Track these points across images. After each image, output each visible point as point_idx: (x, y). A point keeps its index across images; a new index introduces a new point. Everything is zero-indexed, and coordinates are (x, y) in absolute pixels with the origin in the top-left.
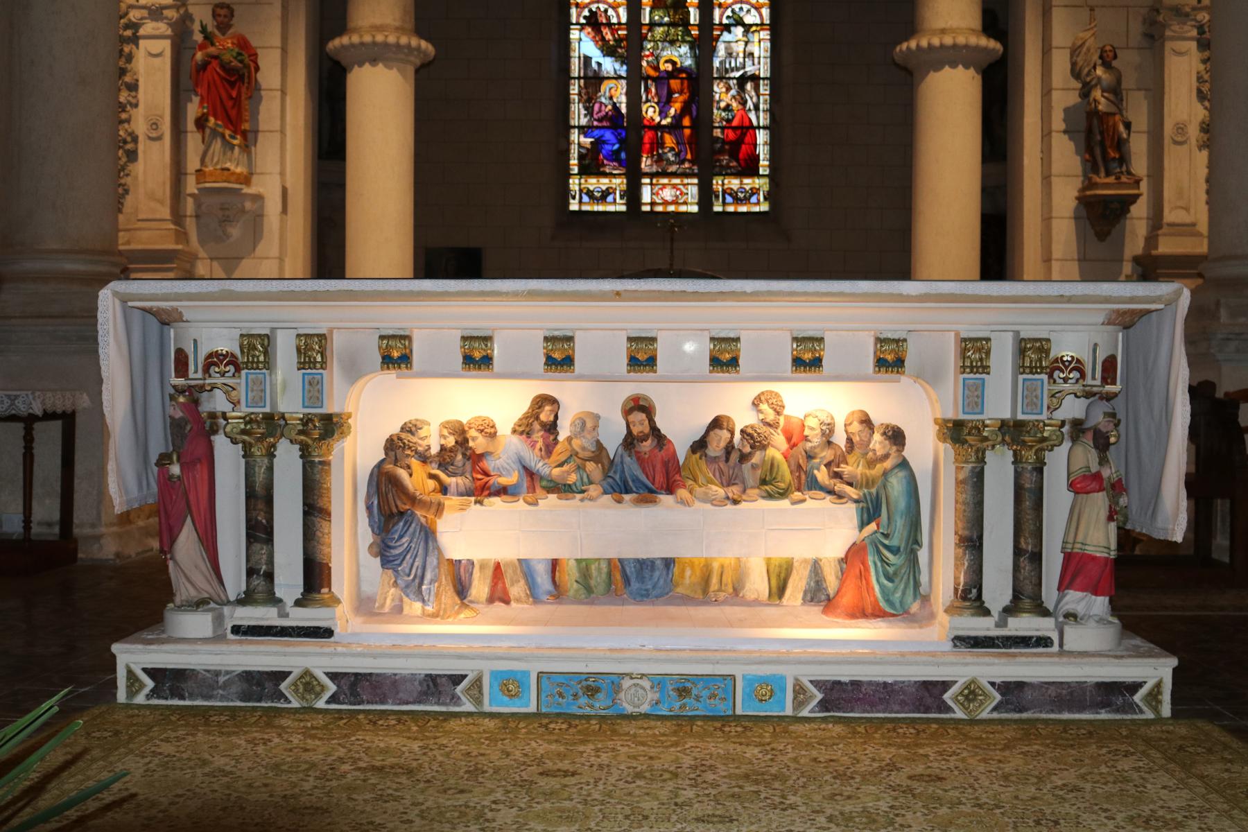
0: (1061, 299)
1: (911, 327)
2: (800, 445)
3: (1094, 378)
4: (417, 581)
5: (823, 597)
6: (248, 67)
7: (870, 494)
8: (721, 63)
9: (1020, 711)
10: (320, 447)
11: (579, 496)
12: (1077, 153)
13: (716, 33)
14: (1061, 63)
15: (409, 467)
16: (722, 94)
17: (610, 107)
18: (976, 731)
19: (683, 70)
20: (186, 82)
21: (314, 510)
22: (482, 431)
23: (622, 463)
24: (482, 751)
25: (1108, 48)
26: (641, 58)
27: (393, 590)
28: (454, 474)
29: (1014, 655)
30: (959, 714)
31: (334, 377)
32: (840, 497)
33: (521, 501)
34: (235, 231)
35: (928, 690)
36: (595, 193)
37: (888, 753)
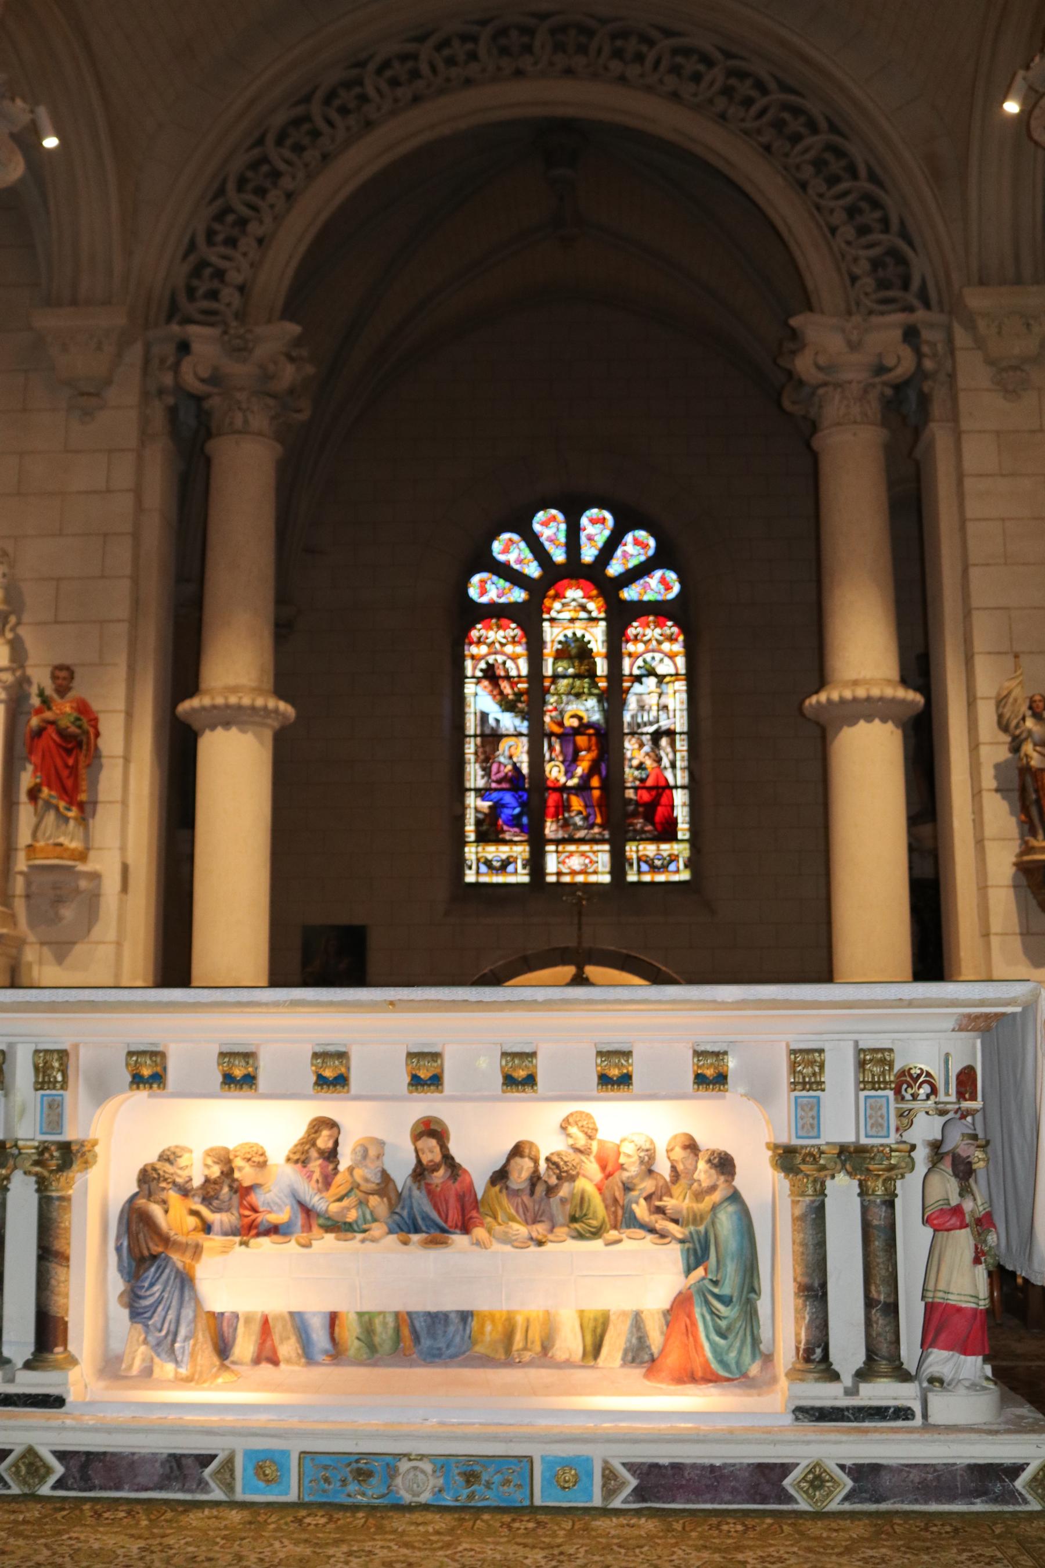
0: (900, 1003)
1: (732, 1038)
2: (617, 1175)
3: (947, 1094)
4: (170, 1338)
5: (646, 1357)
6: (87, 733)
7: (698, 1232)
8: (633, 717)
9: (877, 1501)
10: (58, 1180)
11: (359, 1236)
12: (1012, 813)
13: (626, 685)
14: (986, 714)
15: (164, 1202)
16: (634, 751)
17: (509, 767)
18: (817, 1529)
19: (590, 725)
20: (20, 749)
21: (49, 1254)
22: (249, 1160)
23: (410, 1196)
24: (211, 1555)
25: (1037, 698)
26: (543, 713)
27: (143, 1348)
28: (218, 1210)
29: (866, 1431)
30: (803, 1505)
31: (76, 1098)
32: (663, 1236)
33: (293, 1242)
34: (68, 913)
35: (764, 1475)
36: (494, 862)
37: (699, 1558)
